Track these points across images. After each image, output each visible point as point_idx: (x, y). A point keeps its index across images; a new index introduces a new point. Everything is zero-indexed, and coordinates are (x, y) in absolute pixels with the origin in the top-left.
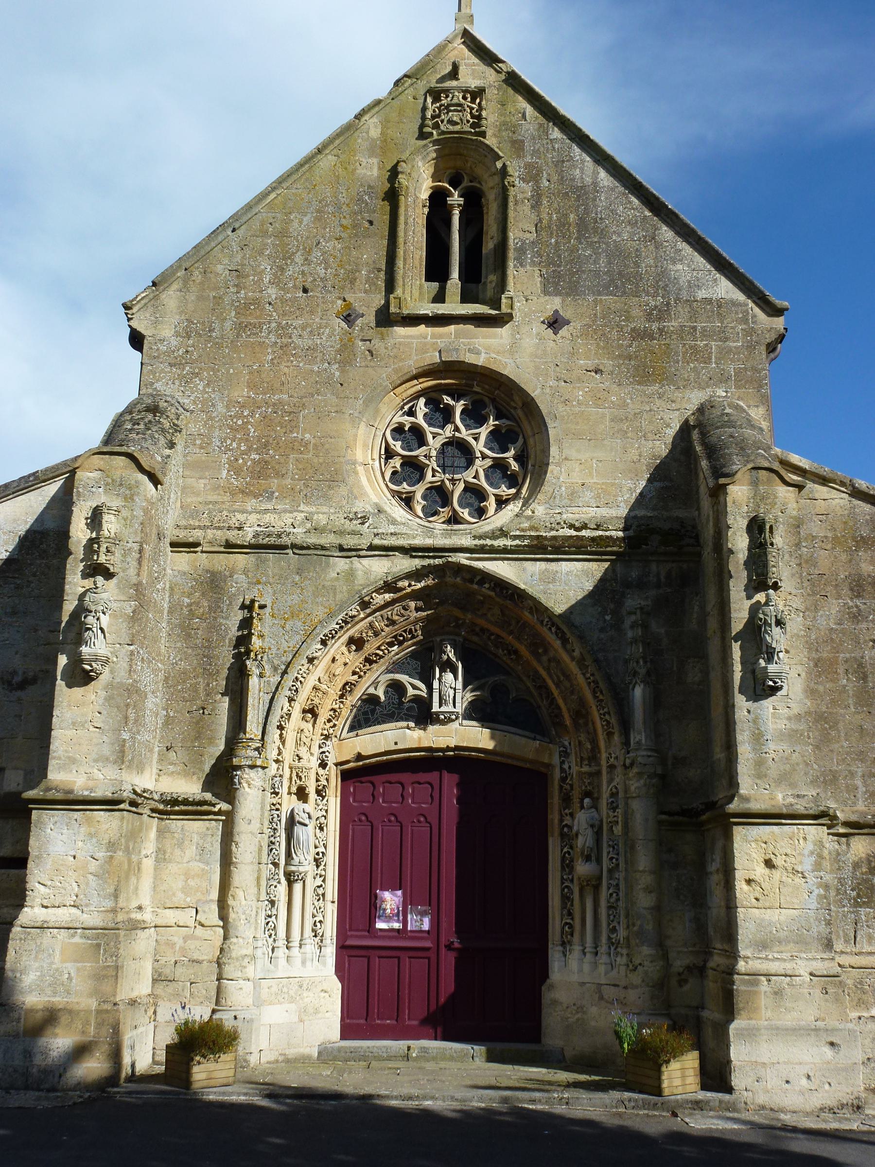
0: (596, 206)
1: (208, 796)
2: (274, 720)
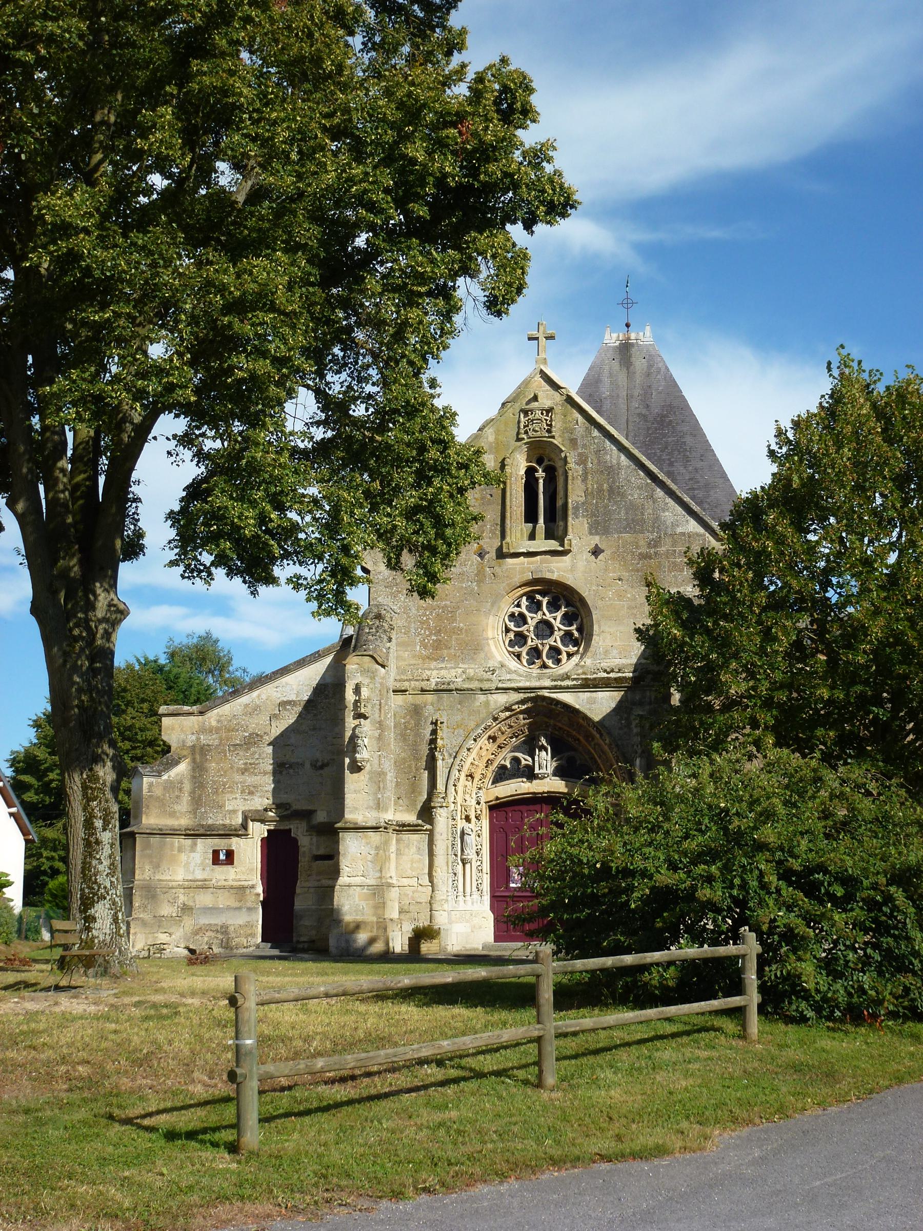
0: (619, 478)
1: (420, 822)
2: (451, 782)
